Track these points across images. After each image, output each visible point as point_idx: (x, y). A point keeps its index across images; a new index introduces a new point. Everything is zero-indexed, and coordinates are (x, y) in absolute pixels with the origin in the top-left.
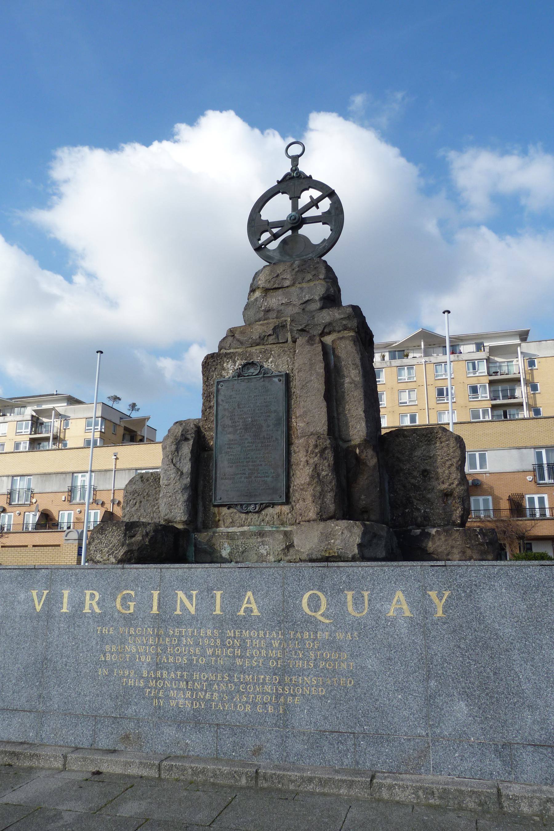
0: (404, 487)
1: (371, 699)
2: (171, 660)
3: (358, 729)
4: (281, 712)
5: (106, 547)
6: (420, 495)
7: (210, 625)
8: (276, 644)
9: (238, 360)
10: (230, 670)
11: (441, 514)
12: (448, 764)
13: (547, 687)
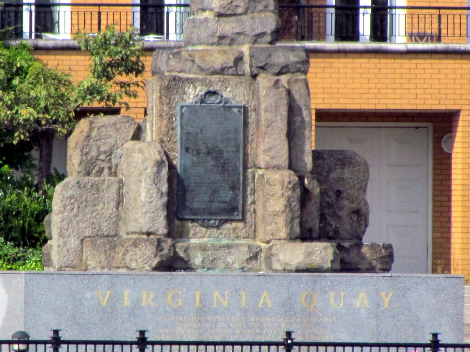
5: (140, 258)
9: (198, 85)
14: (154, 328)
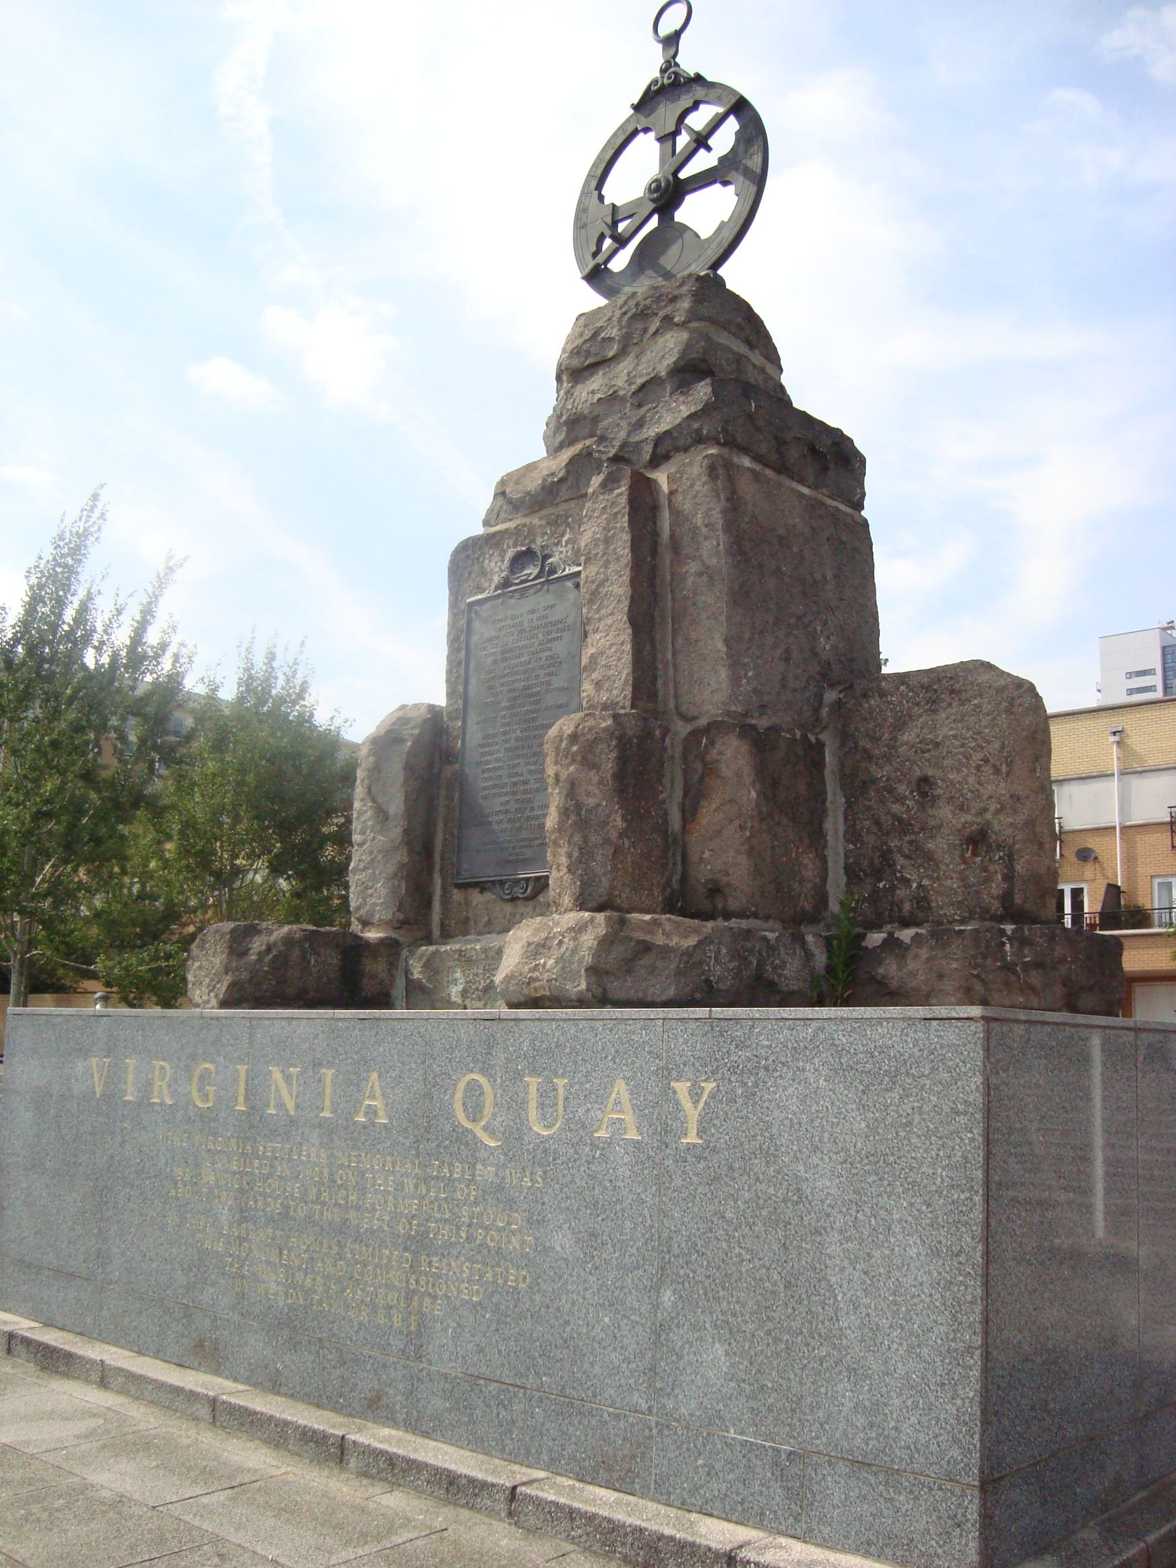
0: (878, 823)
1: (557, 1319)
3: (531, 1381)
4: (412, 1328)
6: (911, 842)
10: (341, 1233)
11: (956, 892)
12: (684, 1479)
13: (891, 1326)
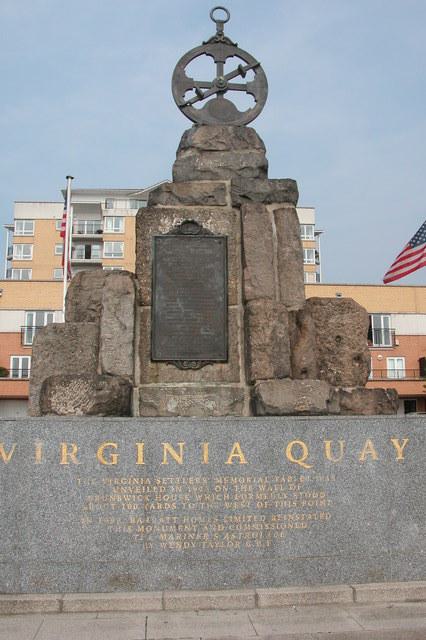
2: (160, 506)
7: (199, 473)
8: (262, 488)
14: (78, 494)
